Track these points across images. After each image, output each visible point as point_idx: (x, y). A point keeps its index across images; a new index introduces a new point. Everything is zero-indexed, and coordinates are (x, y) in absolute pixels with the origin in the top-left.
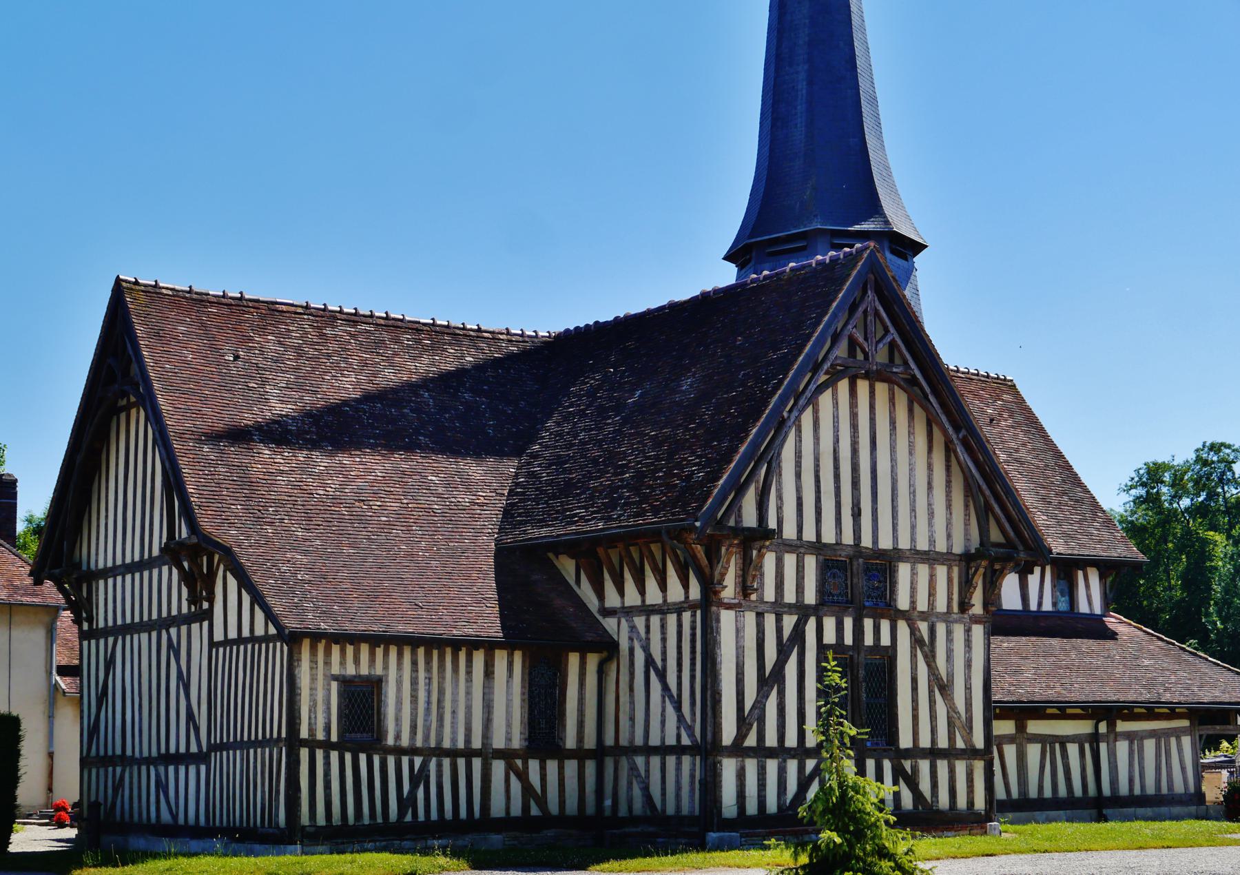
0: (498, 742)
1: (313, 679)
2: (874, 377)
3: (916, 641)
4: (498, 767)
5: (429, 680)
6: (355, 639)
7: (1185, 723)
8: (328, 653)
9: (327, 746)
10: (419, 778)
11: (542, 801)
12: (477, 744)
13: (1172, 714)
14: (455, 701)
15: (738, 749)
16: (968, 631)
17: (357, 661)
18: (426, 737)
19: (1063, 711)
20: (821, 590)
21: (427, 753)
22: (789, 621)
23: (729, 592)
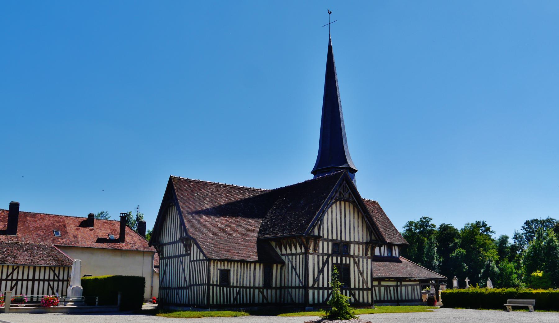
0: (257, 285)
1: (214, 270)
2: (345, 201)
3: (355, 262)
4: (257, 291)
5: (241, 270)
6: (224, 260)
7: (418, 283)
8: (217, 263)
9: (217, 285)
10: (238, 293)
11: (267, 299)
12: (252, 285)
13: (415, 281)
14: (247, 275)
15: (313, 288)
16: (367, 260)
17: (224, 266)
18: (240, 284)
19: (389, 280)
20: (333, 250)
21: (240, 287)
23: (311, 250)
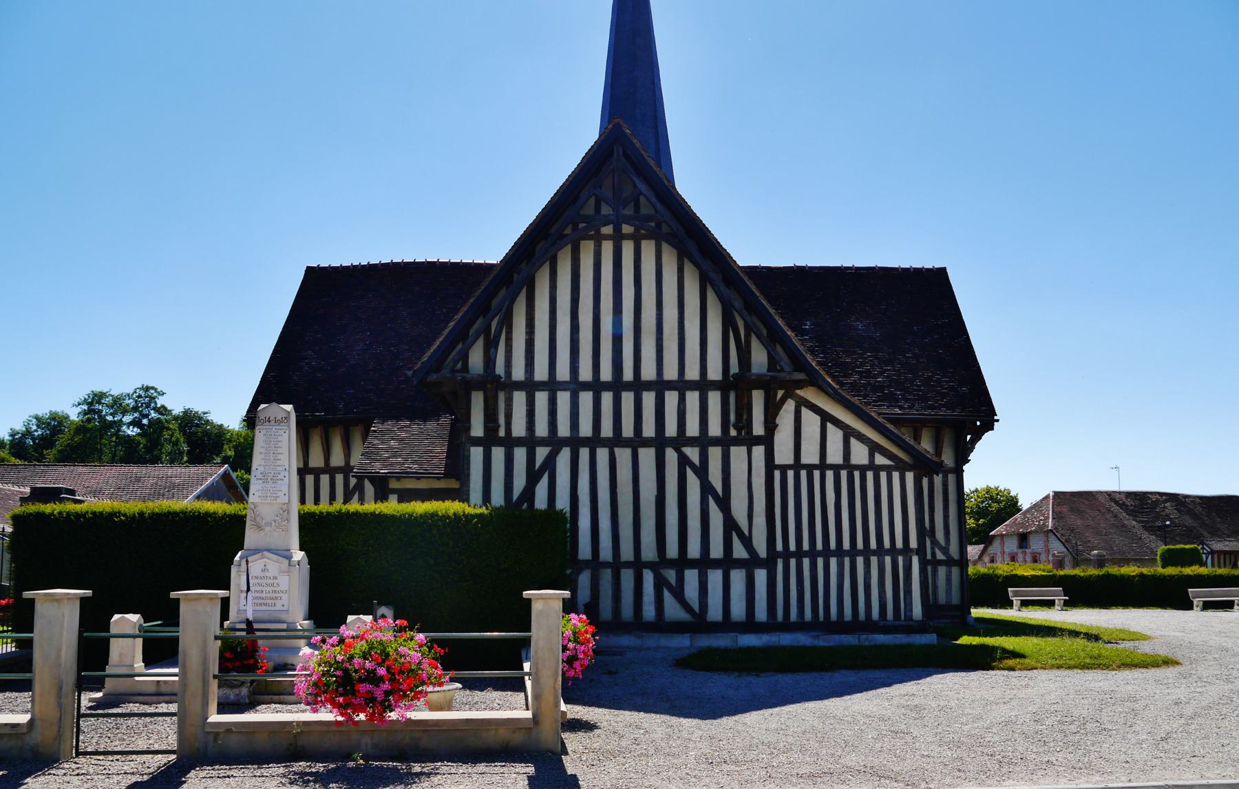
22: (542, 453)
